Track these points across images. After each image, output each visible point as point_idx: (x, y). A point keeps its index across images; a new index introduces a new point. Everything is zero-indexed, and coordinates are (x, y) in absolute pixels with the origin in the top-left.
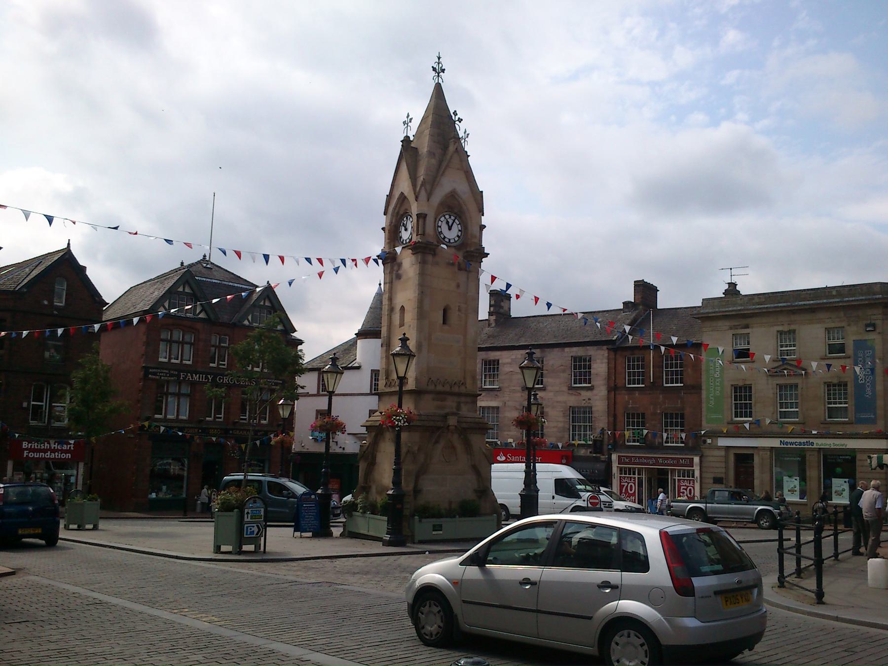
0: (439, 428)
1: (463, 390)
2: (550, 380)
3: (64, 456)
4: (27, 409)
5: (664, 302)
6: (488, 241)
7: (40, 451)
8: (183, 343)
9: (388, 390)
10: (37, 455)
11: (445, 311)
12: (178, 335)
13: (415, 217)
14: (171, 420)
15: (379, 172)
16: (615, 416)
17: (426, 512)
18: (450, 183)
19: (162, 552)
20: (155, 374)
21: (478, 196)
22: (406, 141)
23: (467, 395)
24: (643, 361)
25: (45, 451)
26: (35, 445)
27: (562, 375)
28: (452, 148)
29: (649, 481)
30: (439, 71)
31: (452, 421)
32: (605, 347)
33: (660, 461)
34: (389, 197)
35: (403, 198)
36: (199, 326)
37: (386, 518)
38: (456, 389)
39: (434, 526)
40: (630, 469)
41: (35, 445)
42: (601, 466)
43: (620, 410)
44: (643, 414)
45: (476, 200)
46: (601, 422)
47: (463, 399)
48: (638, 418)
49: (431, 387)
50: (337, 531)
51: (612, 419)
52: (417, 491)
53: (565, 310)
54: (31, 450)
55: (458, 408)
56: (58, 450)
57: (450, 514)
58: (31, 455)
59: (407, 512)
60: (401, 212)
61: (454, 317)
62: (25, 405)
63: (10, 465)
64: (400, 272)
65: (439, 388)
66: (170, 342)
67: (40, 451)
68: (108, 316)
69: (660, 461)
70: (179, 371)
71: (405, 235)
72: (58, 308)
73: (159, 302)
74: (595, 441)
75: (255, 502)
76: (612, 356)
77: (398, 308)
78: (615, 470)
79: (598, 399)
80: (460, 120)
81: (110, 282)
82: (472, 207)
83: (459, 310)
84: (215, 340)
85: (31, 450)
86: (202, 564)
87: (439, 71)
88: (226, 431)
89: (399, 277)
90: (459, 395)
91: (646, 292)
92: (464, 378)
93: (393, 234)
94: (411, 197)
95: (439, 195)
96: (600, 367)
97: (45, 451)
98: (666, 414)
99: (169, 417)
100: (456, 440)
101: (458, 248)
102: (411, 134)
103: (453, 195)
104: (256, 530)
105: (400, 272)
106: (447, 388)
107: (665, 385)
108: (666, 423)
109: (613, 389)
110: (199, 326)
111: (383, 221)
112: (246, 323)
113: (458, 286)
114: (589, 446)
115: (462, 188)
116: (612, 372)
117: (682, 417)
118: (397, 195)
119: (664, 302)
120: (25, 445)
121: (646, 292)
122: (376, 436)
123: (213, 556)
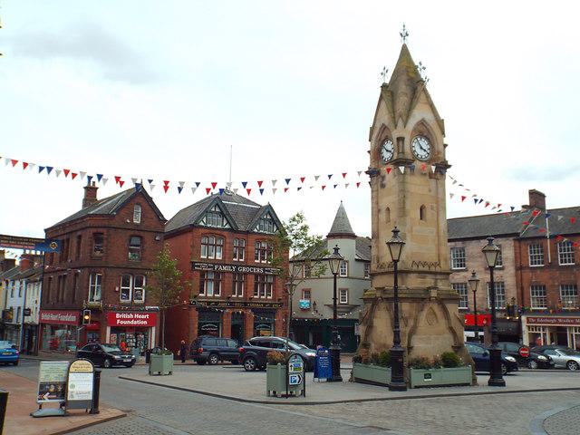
0: (423, 299)
1: (438, 269)
2: (471, 264)
3: (142, 323)
4: (119, 291)
5: (550, 205)
6: (450, 156)
7: (127, 319)
8: (215, 245)
9: (379, 271)
10: (125, 323)
11: (422, 209)
12: (213, 240)
13: (395, 141)
14: (210, 298)
15: (364, 108)
16: (522, 288)
17: (420, 364)
18: (419, 113)
19: (251, 404)
20: (199, 266)
21: (440, 123)
22: (384, 87)
23: (441, 273)
24: (541, 247)
25: (130, 320)
26: (124, 316)
27: (480, 259)
28: (419, 88)
29: (551, 334)
30: (404, 35)
31: (434, 294)
32: (511, 239)
33: (560, 321)
34: (372, 130)
35: (384, 128)
36: (225, 234)
37: (390, 369)
38: (433, 269)
39: (425, 375)
40: (536, 327)
41: (124, 316)
42: (514, 325)
43: (525, 285)
44: (544, 287)
45: (440, 126)
46: (512, 292)
47: (438, 277)
48: (540, 288)
49: (415, 268)
50: (345, 375)
51: (519, 291)
52: (410, 348)
53: (512, 208)
54: (122, 319)
55: (436, 283)
56: (138, 319)
57: (436, 365)
58: (122, 322)
59: (405, 364)
60: (383, 138)
61: (429, 214)
62: (117, 289)
63: (108, 329)
64: (384, 182)
65: (421, 268)
66: (207, 245)
67: (127, 319)
68: (168, 229)
69: (560, 321)
70: (214, 264)
71: (387, 155)
72: (136, 225)
73: (200, 217)
74: (509, 307)
75: (296, 357)
76: (518, 245)
77: (384, 210)
78: (524, 327)
79: (508, 276)
80: (424, 68)
81: (169, 206)
82: (437, 131)
83: (432, 209)
84: (236, 243)
85: (122, 319)
86: (261, 406)
87: (404, 35)
88: (246, 304)
89: (383, 186)
90: (435, 273)
91: (537, 197)
92: (439, 260)
93: (376, 154)
94: (391, 126)
95: (412, 123)
96: (508, 251)
97: (130, 320)
98: (532, 287)
99: (208, 295)
100: (436, 308)
101: (429, 162)
102: (387, 81)
103: (422, 123)
104: (297, 379)
105: (384, 182)
106: (426, 269)
107: (560, 264)
108: (563, 292)
109: (520, 268)
110: (225, 234)
111: (368, 146)
112: (256, 230)
113: (430, 191)
114: (503, 311)
115: (429, 117)
116: (518, 257)
117: (576, 287)
118: (378, 125)
119: (550, 205)
120: (118, 316)
121: (537, 197)
122: (373, 306)
123: (268, 399)
